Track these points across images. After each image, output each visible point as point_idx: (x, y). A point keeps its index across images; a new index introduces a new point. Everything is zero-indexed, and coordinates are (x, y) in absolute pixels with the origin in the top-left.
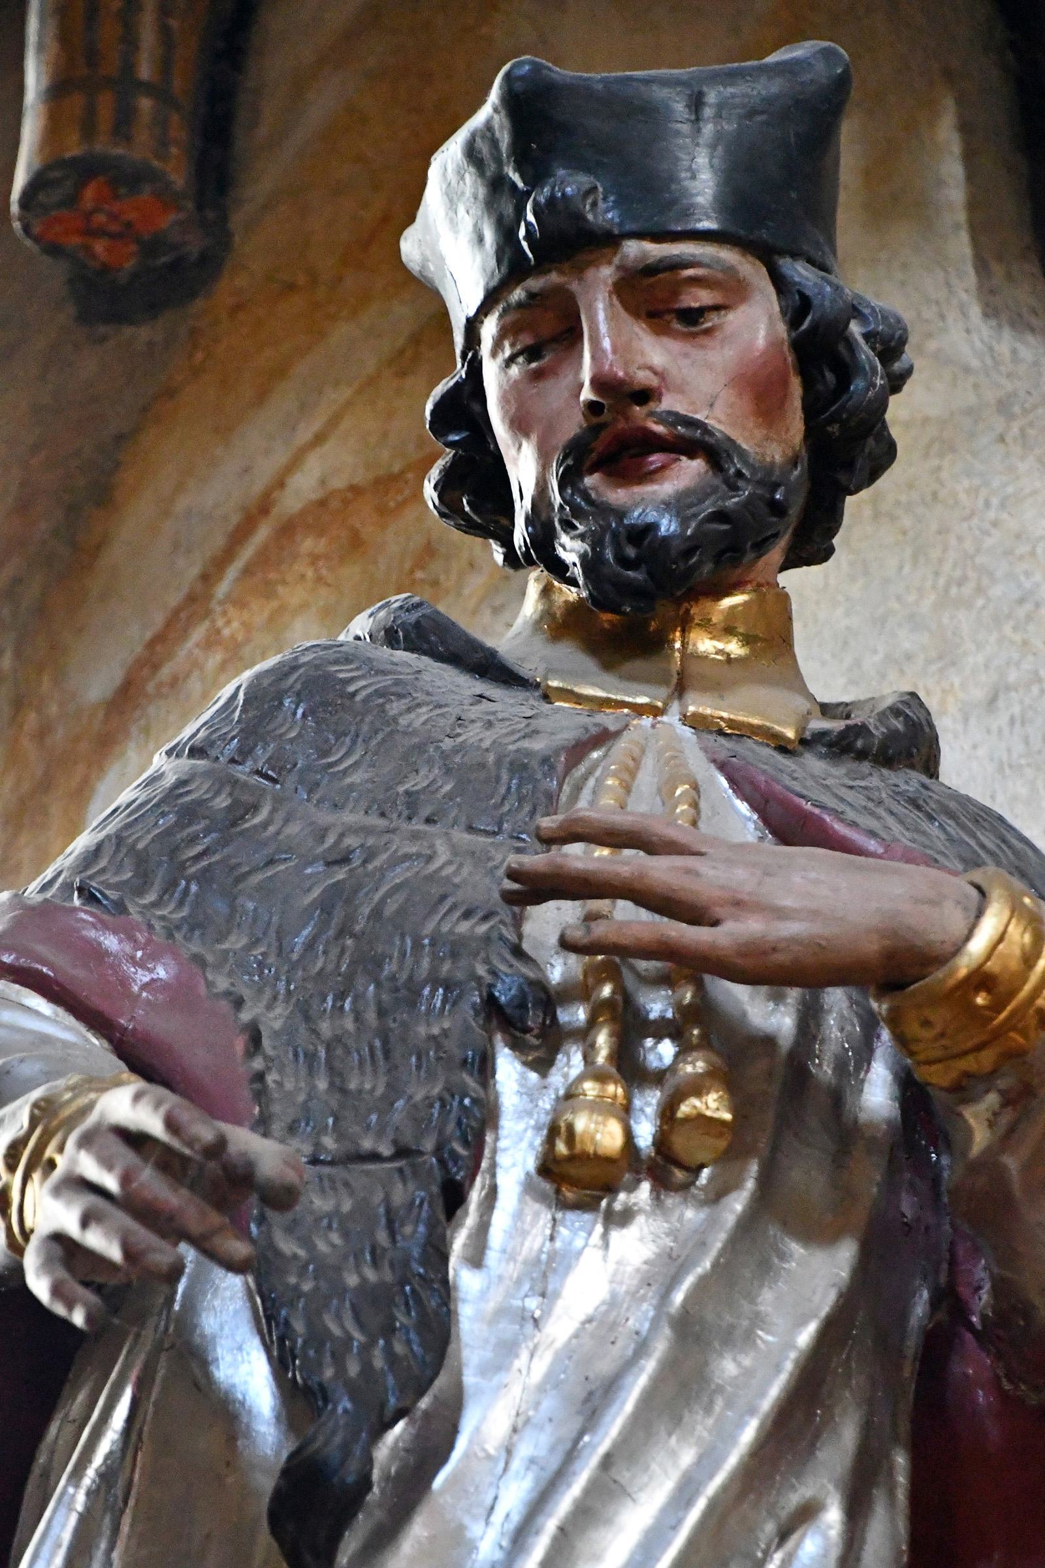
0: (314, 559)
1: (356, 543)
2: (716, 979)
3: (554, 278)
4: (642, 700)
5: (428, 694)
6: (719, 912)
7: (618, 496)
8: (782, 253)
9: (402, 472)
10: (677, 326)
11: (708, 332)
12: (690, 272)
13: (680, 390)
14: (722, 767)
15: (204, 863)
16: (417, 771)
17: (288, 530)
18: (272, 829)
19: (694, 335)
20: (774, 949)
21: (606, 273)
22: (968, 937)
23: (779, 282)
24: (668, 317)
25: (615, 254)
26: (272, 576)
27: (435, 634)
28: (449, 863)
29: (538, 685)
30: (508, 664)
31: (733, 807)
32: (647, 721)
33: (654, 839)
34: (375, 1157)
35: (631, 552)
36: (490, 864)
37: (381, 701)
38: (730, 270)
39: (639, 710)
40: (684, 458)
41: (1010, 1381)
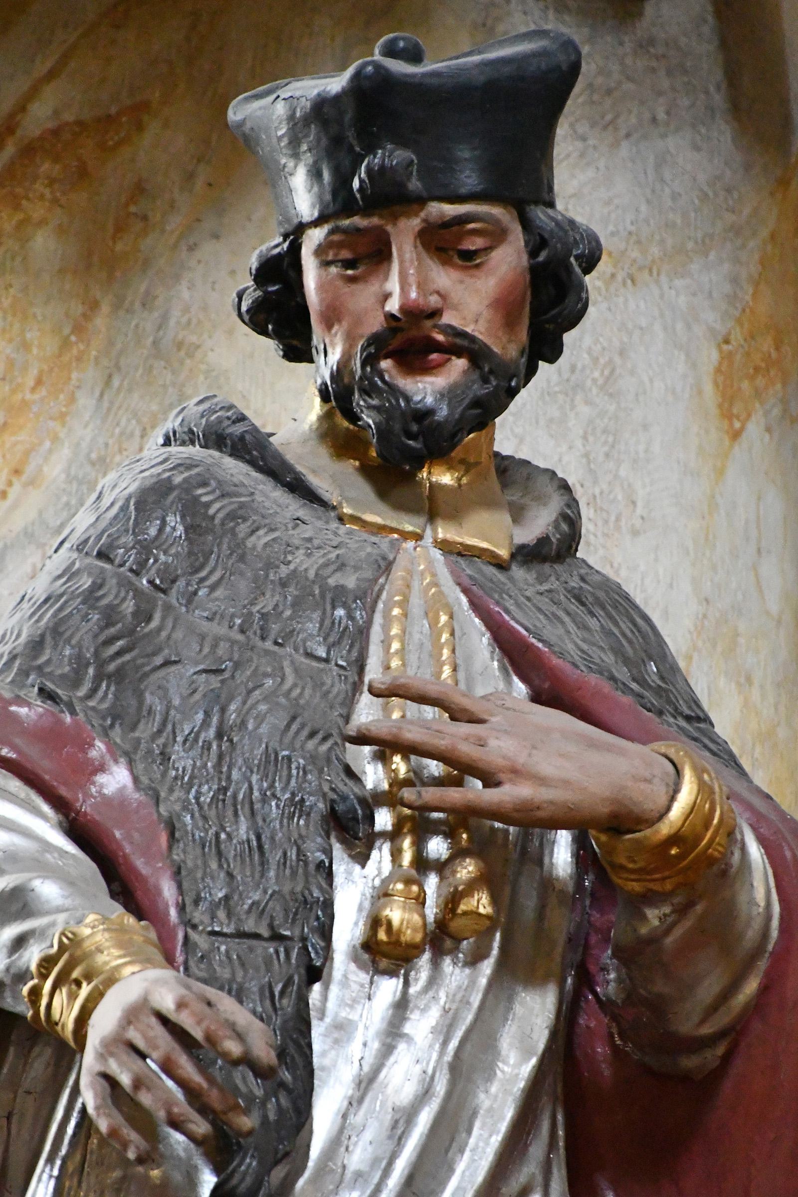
0: (52, 182)
1: (83, 173)
2: (471, 778)
3: (375, 221)
4: (409, 528)
5: (263, 517)
6: (502, 776)
7: (406, 383)
8: (529, 202)
9: (119, 114)
10: (460, 262)
11: (478, 266)
12: (472, 226)
13: (455, 308)
14: (465, 591)
15: (119, 661)
16: (263, 594)
17: (29, 151)
18: (164, 634)
19: (465, 268)
20: (538, 808)
21: (415, 223)
22: (668, 809)
23: (526, 224)
24: (451, 253)
25: (422, 209)
26: (19, 190)
27: (256, 449)
28: (295, 685)
29: (334, 508)
30: (313, 487)
31: (473, 622)
32: (410, 544)
33: (453, 706)
34: (257, 936)
35: (415, 428)
36: (325, 688)
37: (232, 524)
38: (496, 222)
39: (406, 536)
40: (453, 358)
41: (621, 1038)
